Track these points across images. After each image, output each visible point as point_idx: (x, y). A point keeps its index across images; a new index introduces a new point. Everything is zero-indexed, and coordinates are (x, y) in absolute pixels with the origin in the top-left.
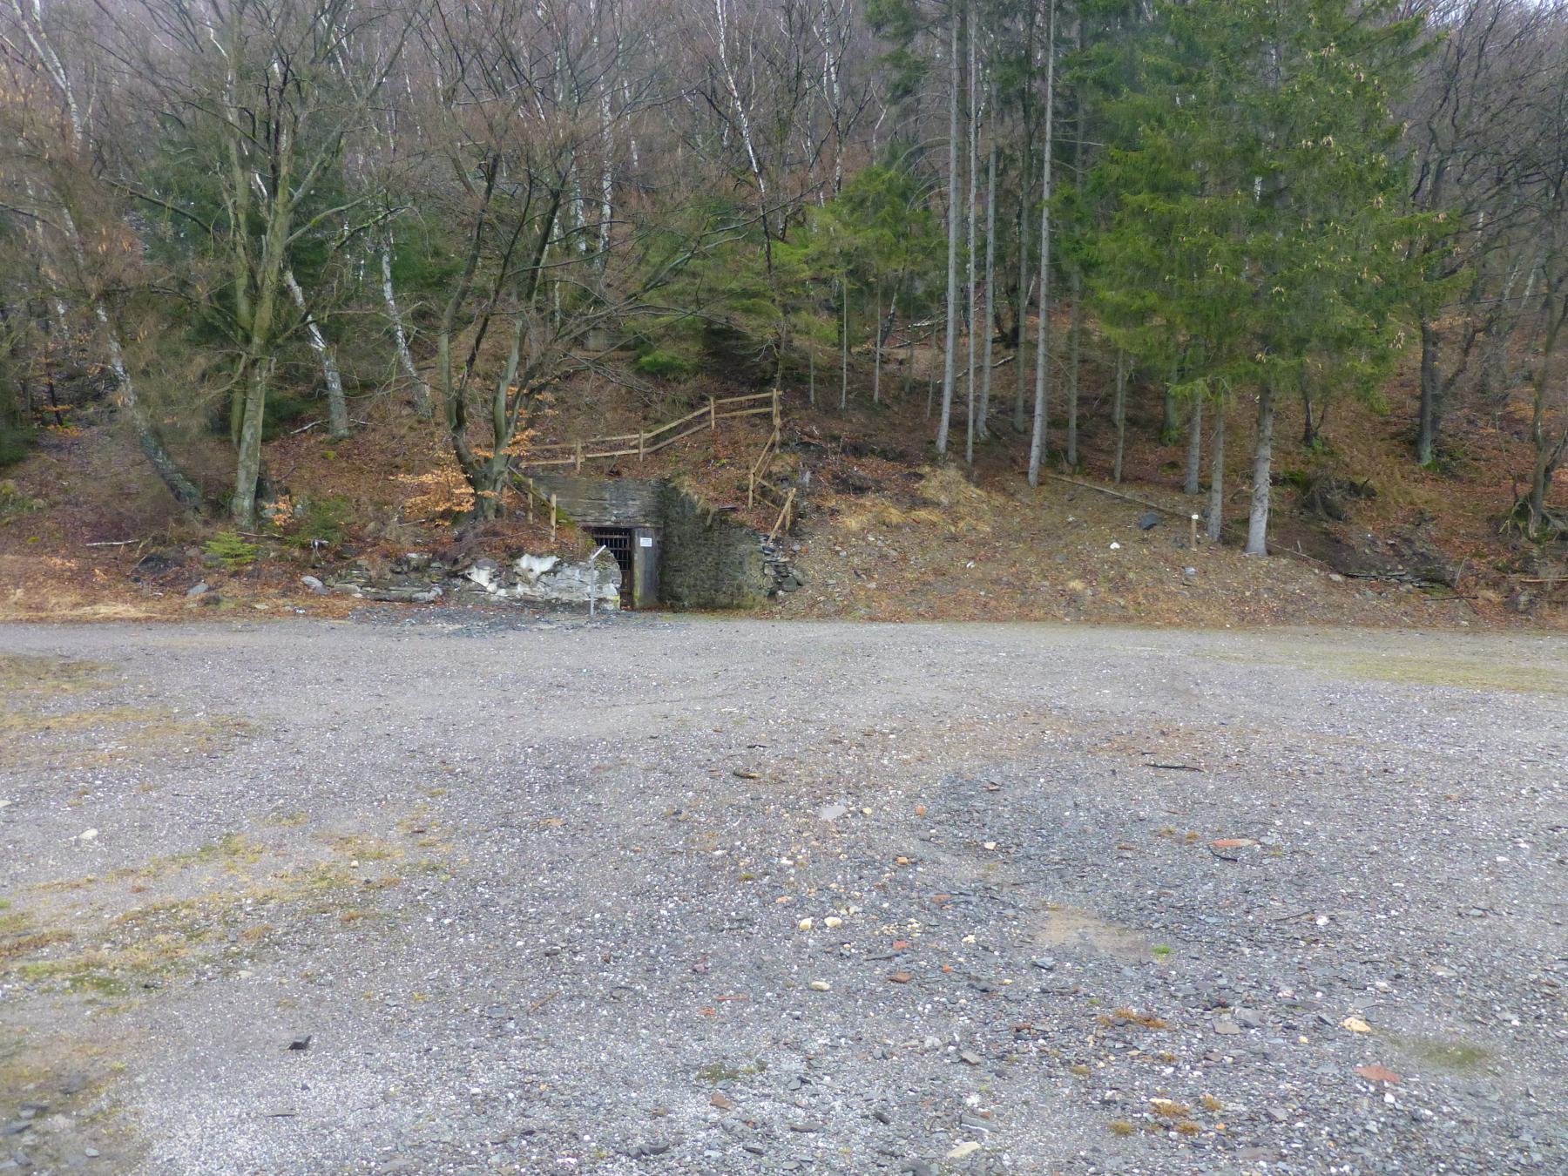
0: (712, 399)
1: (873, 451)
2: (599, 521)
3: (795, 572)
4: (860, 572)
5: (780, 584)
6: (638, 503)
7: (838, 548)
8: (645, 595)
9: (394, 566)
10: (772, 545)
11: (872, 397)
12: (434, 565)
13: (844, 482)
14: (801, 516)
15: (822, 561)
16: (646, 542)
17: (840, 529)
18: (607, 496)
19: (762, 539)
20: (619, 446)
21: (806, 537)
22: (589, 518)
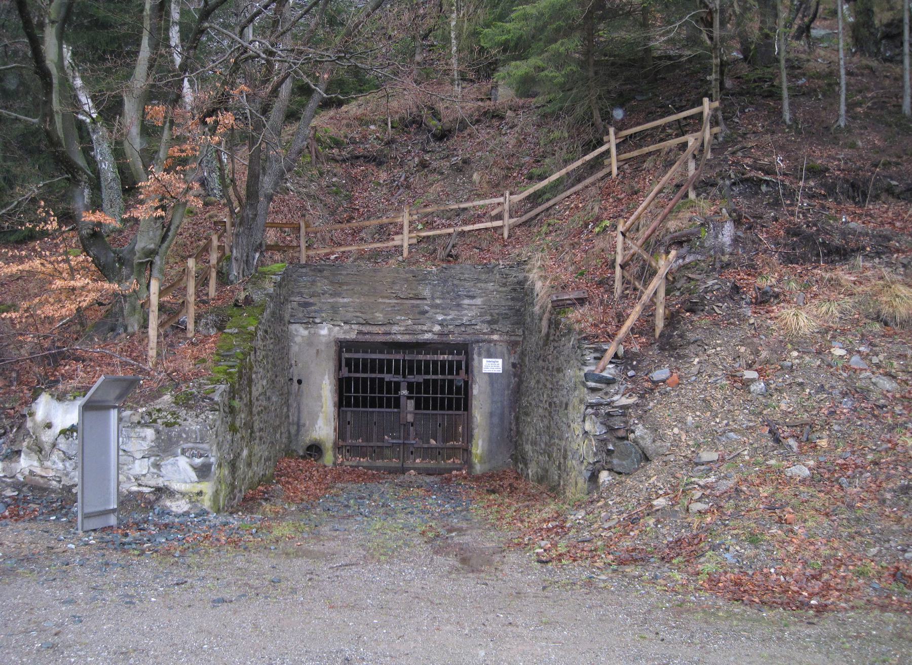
1: (890, 191)
5: (609, 452)
6: (479, 301)
7: (750, 374)
8: (490, 454)
10: (610, 371)
11: (900, 106)
13: (808, 239)
16: (492, 366)
18: (427, 292)
19: (590, 357)
20: (479, 218)
22: (395, 329)
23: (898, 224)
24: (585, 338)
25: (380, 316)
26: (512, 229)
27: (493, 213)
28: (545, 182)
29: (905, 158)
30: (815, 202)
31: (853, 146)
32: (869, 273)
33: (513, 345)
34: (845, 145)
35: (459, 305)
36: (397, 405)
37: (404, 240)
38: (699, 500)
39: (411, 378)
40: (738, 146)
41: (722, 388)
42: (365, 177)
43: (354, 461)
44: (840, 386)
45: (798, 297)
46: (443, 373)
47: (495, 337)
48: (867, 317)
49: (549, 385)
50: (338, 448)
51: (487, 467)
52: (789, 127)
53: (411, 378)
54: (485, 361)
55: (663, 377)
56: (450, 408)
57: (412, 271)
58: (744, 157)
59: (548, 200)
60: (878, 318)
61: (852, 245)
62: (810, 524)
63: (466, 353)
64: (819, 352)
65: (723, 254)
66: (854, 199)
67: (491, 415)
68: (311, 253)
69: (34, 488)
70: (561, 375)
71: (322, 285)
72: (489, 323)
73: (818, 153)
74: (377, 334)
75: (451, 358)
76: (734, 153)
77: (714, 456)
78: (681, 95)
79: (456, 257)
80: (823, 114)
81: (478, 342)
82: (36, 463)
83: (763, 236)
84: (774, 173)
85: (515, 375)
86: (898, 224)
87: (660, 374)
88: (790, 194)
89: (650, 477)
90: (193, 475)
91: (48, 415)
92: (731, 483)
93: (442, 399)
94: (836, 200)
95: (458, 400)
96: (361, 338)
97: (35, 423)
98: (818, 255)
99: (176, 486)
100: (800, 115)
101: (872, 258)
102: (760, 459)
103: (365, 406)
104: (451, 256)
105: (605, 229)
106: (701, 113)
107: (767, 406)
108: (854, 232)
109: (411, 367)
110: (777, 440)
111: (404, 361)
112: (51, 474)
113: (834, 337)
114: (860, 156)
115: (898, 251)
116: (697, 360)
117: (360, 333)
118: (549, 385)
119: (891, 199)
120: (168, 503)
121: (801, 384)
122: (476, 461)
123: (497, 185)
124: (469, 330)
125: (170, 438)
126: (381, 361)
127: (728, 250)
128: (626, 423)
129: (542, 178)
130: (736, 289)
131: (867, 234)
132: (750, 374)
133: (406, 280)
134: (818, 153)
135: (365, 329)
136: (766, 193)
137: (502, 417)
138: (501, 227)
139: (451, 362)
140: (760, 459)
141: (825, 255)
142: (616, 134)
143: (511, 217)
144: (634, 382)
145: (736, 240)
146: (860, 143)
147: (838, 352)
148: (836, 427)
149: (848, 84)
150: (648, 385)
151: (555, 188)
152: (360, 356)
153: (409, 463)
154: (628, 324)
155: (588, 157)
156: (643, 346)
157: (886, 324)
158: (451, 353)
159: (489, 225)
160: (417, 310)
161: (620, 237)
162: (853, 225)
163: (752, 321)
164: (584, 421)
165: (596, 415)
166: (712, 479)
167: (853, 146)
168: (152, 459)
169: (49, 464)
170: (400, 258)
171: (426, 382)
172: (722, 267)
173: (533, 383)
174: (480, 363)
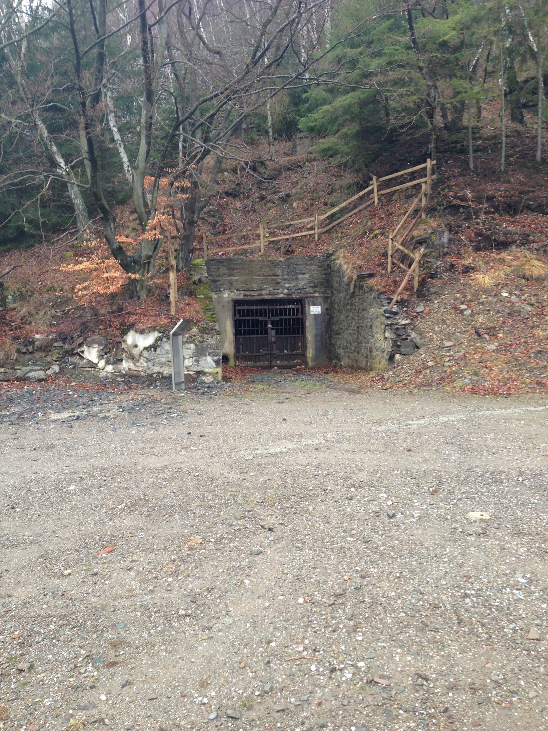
0: (374, 178)
2: (273, 294)
3: (413, 335)
4: (482, 332)
5: (399, 346)
6: (307, 276)
7: (463, 307)
8: (316, 357)
9: (21, 347)
10: (395, 308)
11: (535, 156)
12: (56, 344)
13: (488, 238)
14: (432, 277)
15: (444, 321)
16: (315, 310)
17: (471, 286)
18: (279, 272)
20: (300, 229)
21: (433, 297)
22: (264, 292)
23: (533, 226)
24: (381, 293)
25: (255, 286)
26: (320, 235)
27: (309, 226)
28: (336, 209)
29: (538, 188)
30: (489, 216)
31: (509, 182)
32: (519, 255)
33: (326, 299)
34: (504, 182)
35: (297, 278)
36: (266, 333)
37: (262, 243)
38: (448, 361)
39: (272, 318)
40: (445, 185)
41: (451, 313)
42: (228, 205)
43: (245, 363)
44: (507, 310)
45: (483, 268)
46: (289, 315)
47: (316, 295)
48: (518, 277)
49: (356, 318)
50: (236, 358)
51: (315, 363)
52: (473, 172)
53: (272, 318)
54: (311, 307)
55: (421, 310)
56: (294, 333)
57: (271, 261)
58: (450, 191)
59: (339, 218)
60: (524, 277)
61: (510, 240)
62: (499, 367)
63: (301, 304)
64: (496, 295)
65: (444, 248)
66: (509, 213)
67: (316, 336)
68: (210, 252)
69: (131, 376)
70: (365, 312)
71: (223, 270)
72: (313, 287)
73: (489, 187)
74: (255, 295)
75: (293, 307)
76: (443, 190)
77: (451, 344)
78: (410, 153)
79: (293, 252)
80: (492, 163)
81: (307, 297)
82: (132, 364)
83: (463, 238)
84: (466, 201)
85: (328, 314)
86: (533, 226)
87: (420, 309)
88: (477, 213)
89: (422, 355)
90: (214, 365)
91: (134, 341)
92: (461, 354)
93: (290, 329)
94: (499, 214)
95: (298, 329)
96: (246, 298)
97: (128, 345)
98: (492, 246)
99: (207, 370)
100: (479, 165)
101: (520, 246)
102: (472, 343)
103: (249, 334)
104: (289, 251)
105: (376, 236)
106: (426, 168)
107: (473, 321)
108: (510, 233)
109: (273, 312)
110: (479, 335)
111: (269, 309)
112: (141, 369)
113: (502, 288)
114: (513, 188)
115: (533, 242)
116: (436, 302)
117: (245, 295)
118: (356, 318)
119: (529, 212)
120: (203, 378)
121: (488, 310)
122: (309, 360)
123: (307, 209)
124: (303, 292)
125: (203, 348)
126: (257, 310)
127: (446, 246)
128: (406, 332)
129: (333, 205)
130: (452, 266)
131: (517, 233)
132: (463, 307)
133: (268, 266)
134: (489, 187)
135: (248, 293)
136: (463, 213)
137: (321, 337)
138: (314, 234)
139: (293, 309)
140: (472, 343)
141: (495, 246)
142: (377, 180)
143: (318, 228)
144: (407, 313)
145: (450, 240)
146: (512, 180)
147: (505, 294)
148: (506, 329)
149: (506, 143)
150: (414, 314)
151: (342, 211)
152: (245, 307)
153: (274, 363)
154: (403, 285)
155: (361, 194)
156: (409, 296)
157: (528, 280)
158: (293, 304)
159: (307, 233)
160: (274, 282)
161: (390, 241)
162: (509, 228)
163: (462, 281)
164: (384, 332)
165: (391, 329)
166: (452, 353)
167: (509, 182)
168: (195, 358)
169: (139, 364)
170: (260, 254)
171: (281, 320)
172: (444, 255)
173: (342, 317)
174: (309, 309)
